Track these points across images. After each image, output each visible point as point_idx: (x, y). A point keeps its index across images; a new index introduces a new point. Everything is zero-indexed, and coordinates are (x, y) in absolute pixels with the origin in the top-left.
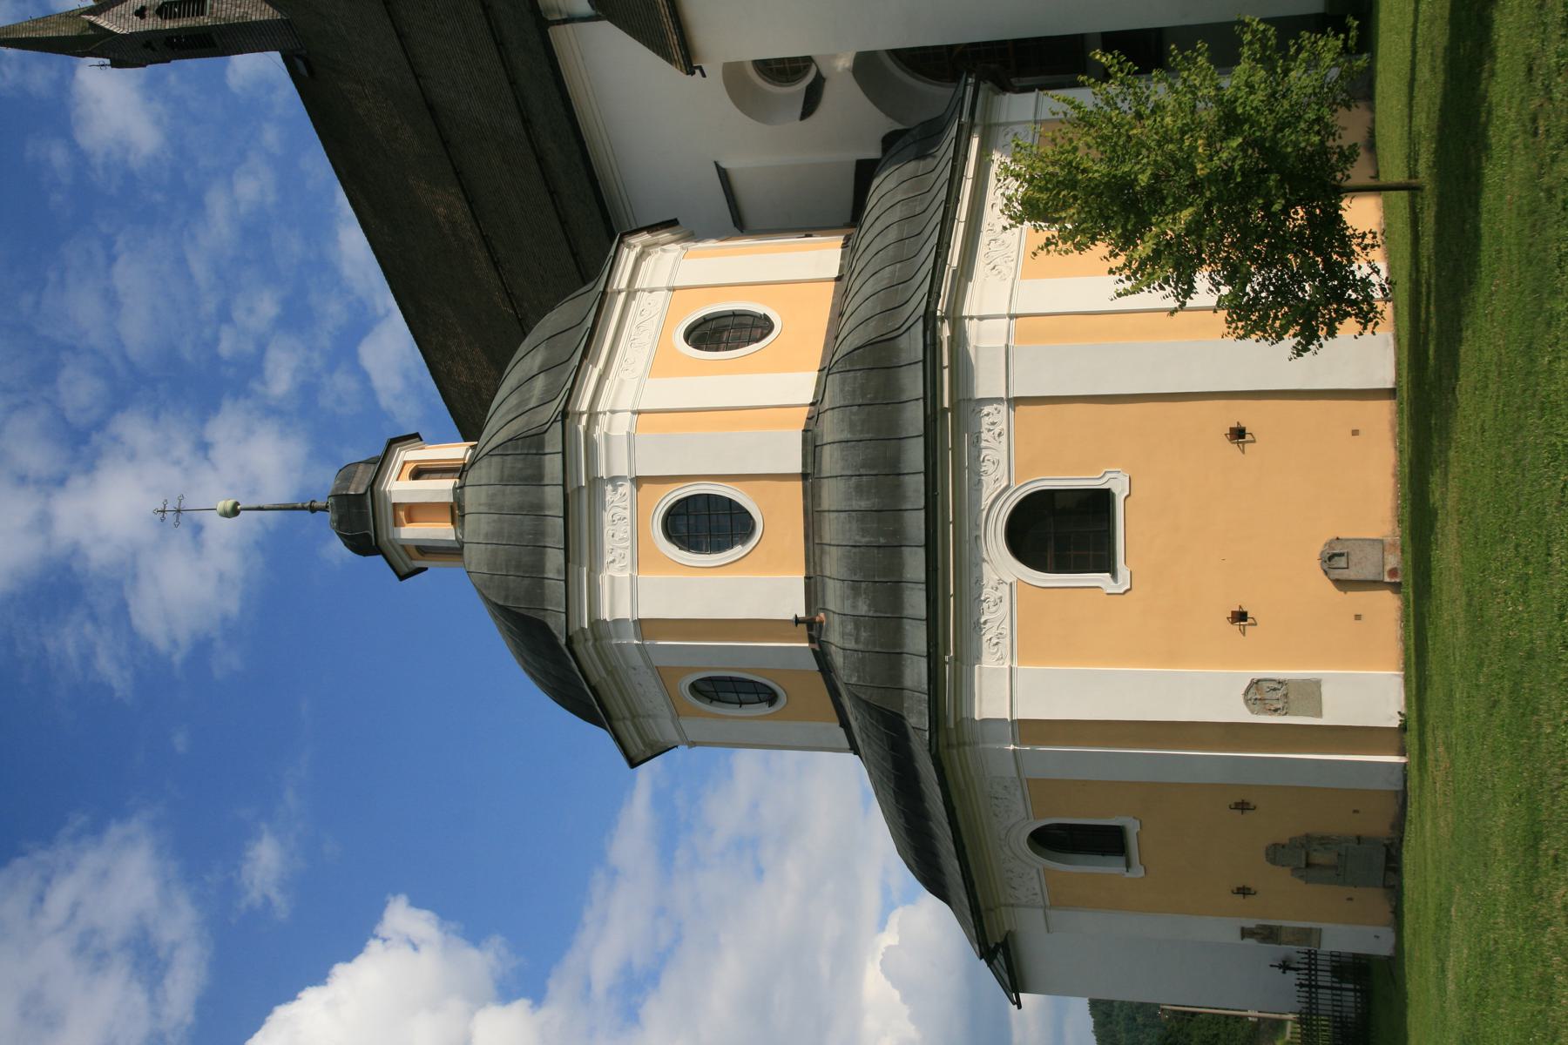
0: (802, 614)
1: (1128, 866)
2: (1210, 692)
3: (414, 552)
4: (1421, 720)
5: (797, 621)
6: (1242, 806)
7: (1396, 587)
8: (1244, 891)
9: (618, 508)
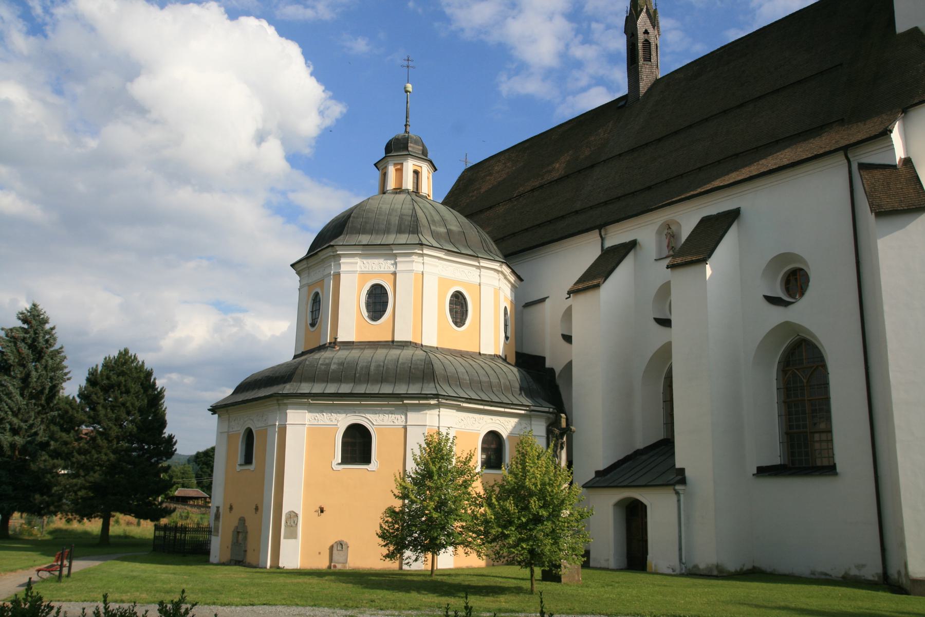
0: (338, 340)
1: (241, 465)
2: (295, 497)
4: (281, 573)
5: (336, 339)
6: (257, 509)
7: (330, 567)
8: (231, 508)
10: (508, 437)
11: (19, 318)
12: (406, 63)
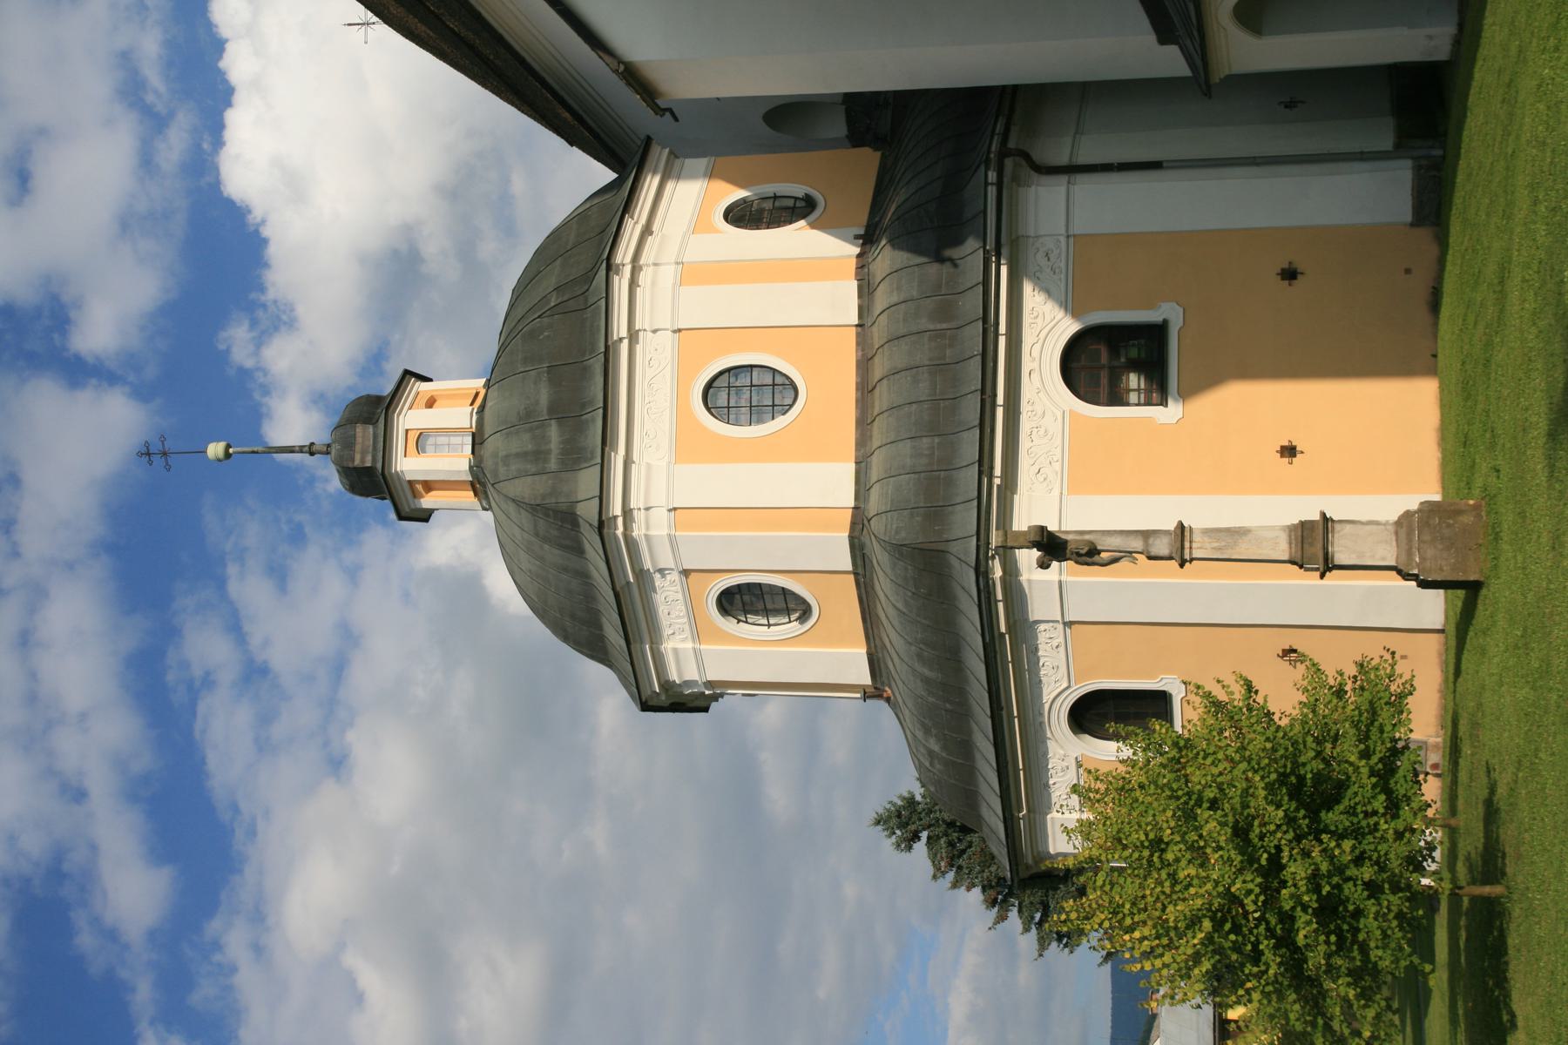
9: (669, 600)
10: (1075, 314)
11: (910, 848)
12: (157, 460)
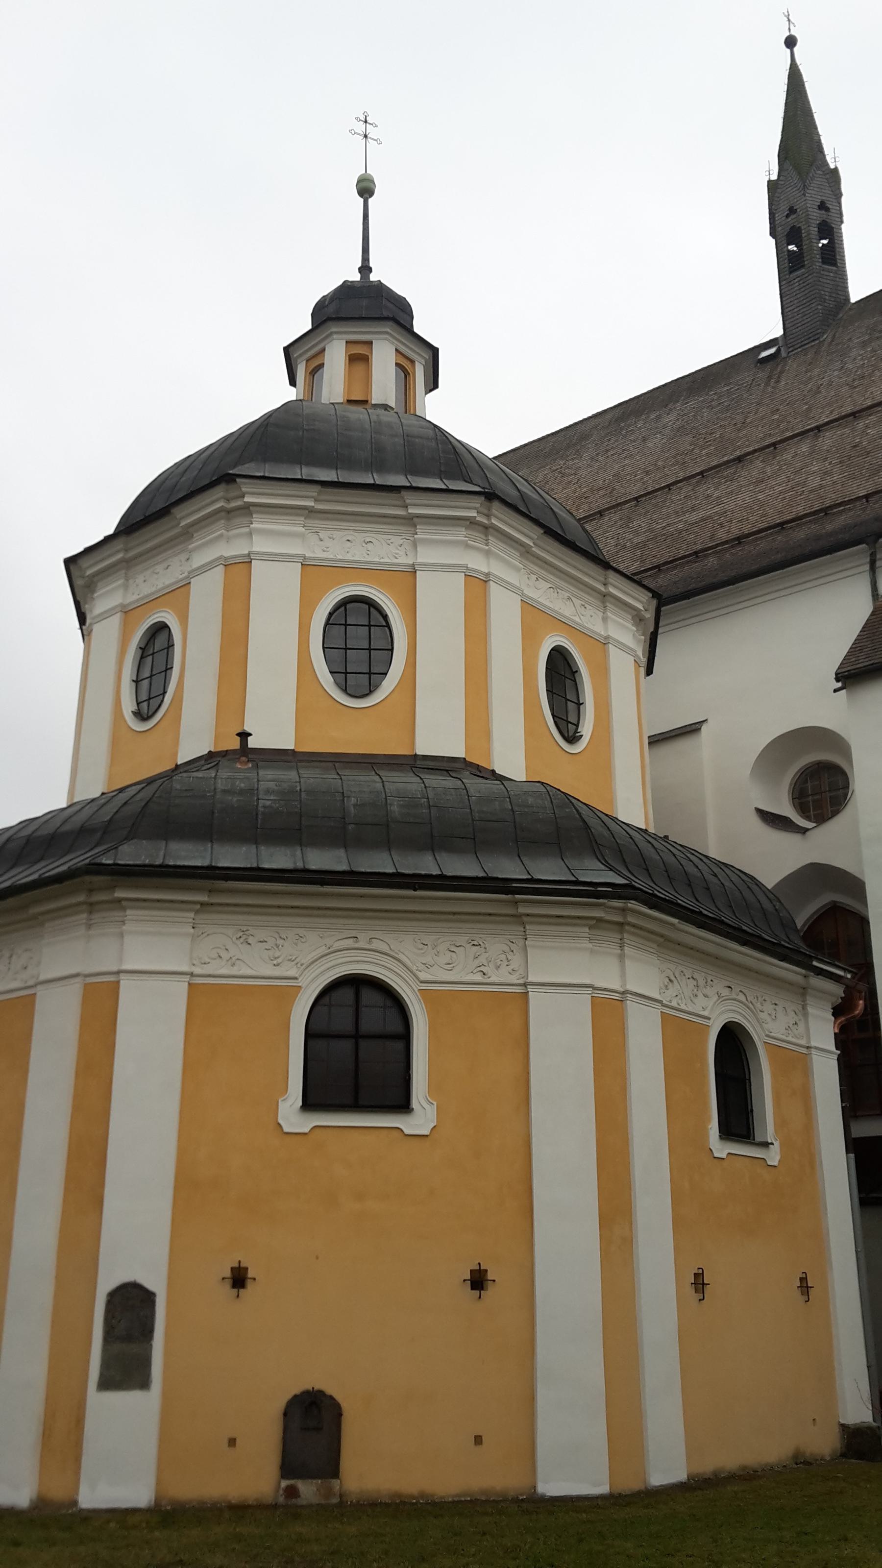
3: (315, 363)
5: (244, 736)
9: (382, 548)
